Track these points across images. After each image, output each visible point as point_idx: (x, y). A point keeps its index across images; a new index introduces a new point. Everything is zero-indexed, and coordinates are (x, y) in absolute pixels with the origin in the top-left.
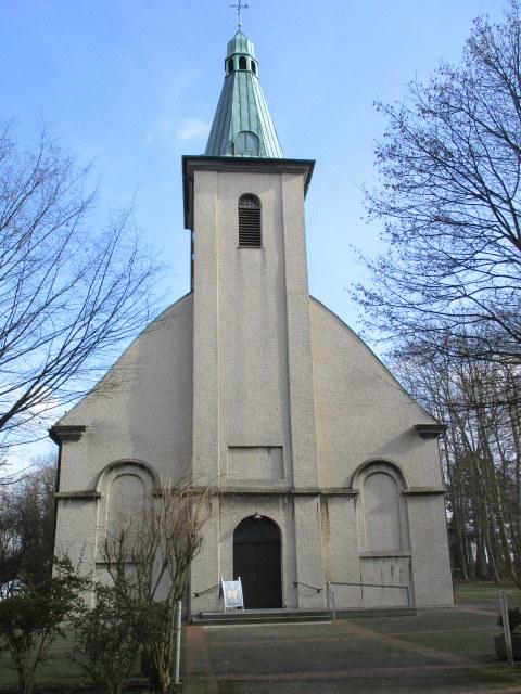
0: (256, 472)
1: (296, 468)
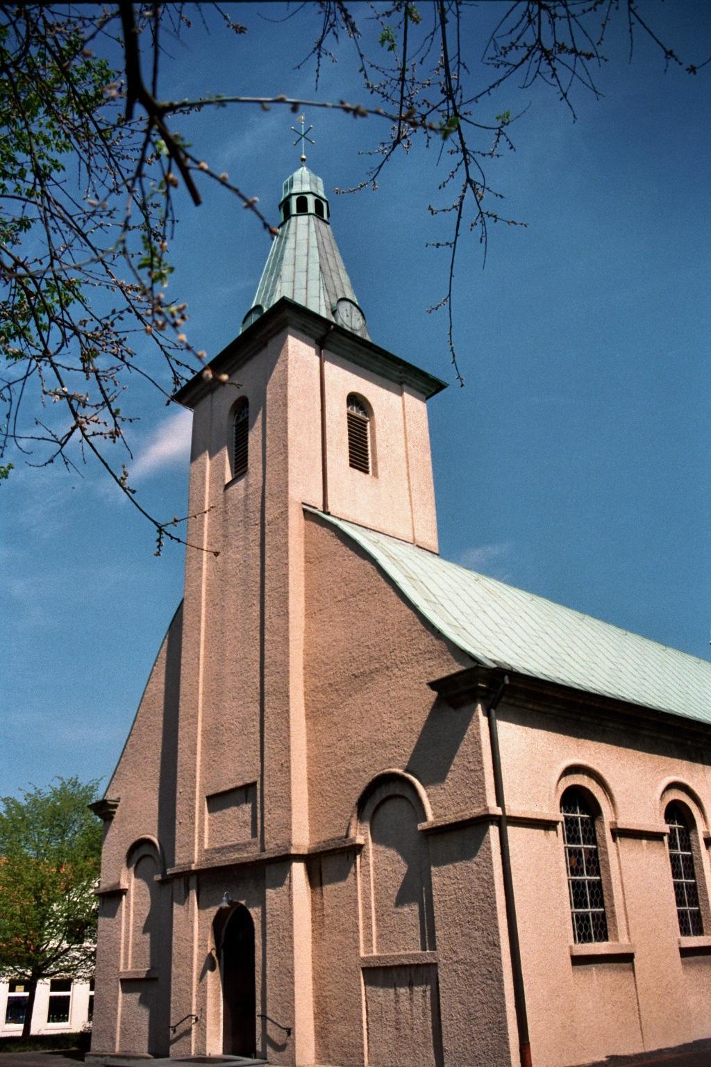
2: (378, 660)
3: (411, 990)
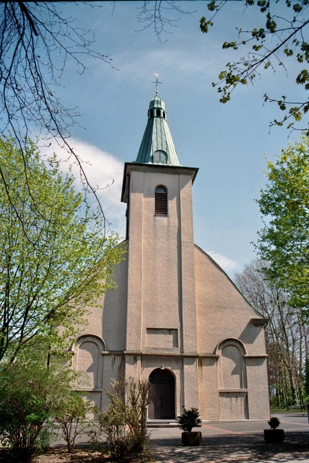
0: (163, 344)
1: (184, 342)
2: (228, 305)
3: (237, 399)
